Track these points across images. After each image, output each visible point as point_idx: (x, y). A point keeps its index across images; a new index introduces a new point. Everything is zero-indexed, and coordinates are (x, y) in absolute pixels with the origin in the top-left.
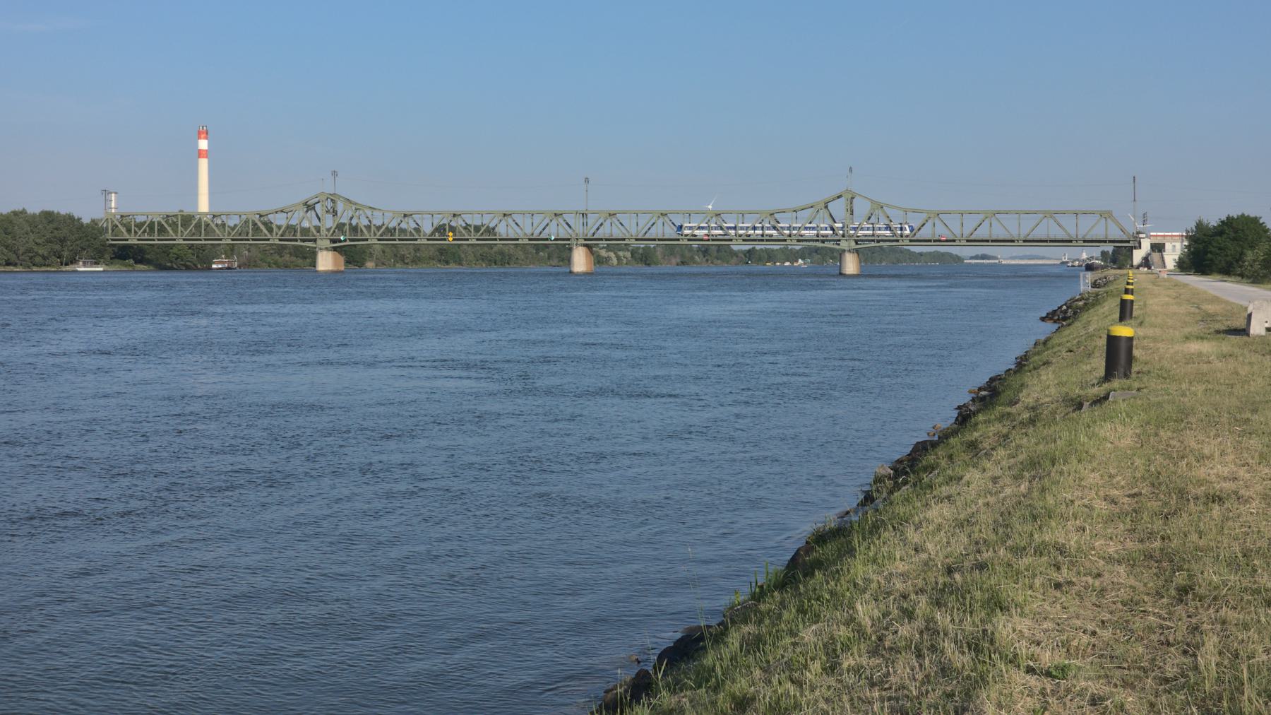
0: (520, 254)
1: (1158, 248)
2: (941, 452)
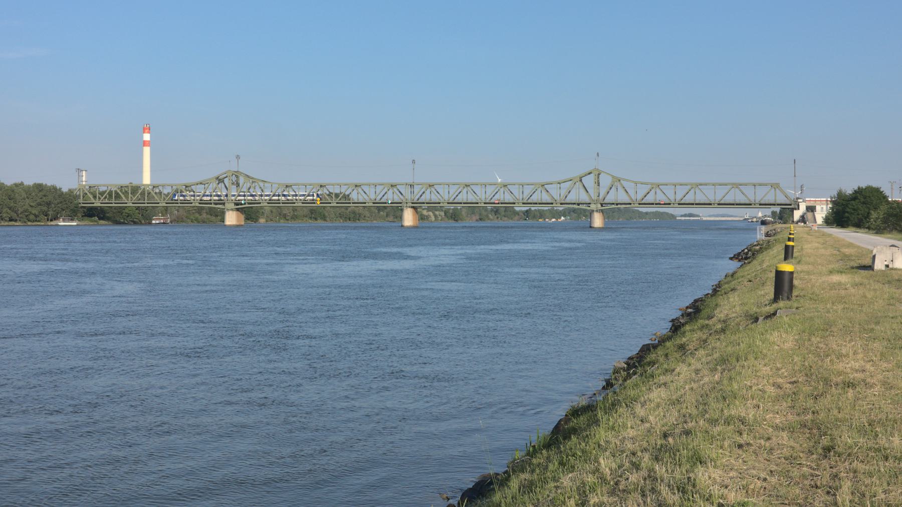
0: (367, 214)
1: (811, 209)
2: (660, 351)
